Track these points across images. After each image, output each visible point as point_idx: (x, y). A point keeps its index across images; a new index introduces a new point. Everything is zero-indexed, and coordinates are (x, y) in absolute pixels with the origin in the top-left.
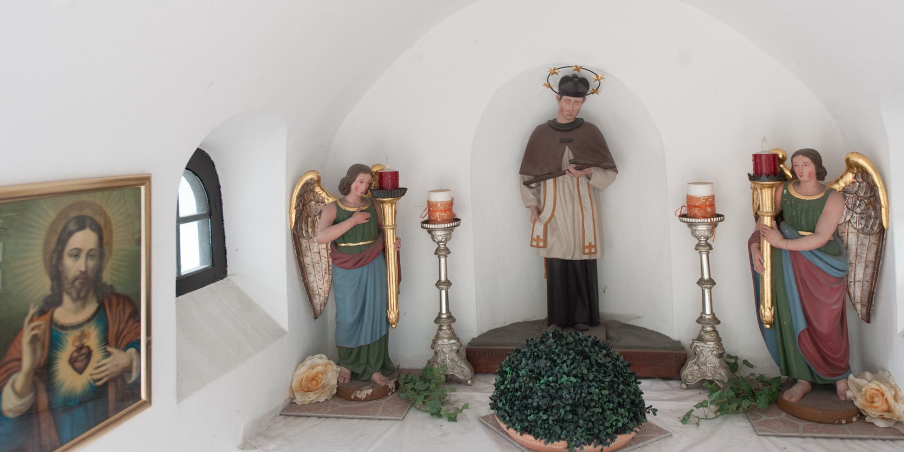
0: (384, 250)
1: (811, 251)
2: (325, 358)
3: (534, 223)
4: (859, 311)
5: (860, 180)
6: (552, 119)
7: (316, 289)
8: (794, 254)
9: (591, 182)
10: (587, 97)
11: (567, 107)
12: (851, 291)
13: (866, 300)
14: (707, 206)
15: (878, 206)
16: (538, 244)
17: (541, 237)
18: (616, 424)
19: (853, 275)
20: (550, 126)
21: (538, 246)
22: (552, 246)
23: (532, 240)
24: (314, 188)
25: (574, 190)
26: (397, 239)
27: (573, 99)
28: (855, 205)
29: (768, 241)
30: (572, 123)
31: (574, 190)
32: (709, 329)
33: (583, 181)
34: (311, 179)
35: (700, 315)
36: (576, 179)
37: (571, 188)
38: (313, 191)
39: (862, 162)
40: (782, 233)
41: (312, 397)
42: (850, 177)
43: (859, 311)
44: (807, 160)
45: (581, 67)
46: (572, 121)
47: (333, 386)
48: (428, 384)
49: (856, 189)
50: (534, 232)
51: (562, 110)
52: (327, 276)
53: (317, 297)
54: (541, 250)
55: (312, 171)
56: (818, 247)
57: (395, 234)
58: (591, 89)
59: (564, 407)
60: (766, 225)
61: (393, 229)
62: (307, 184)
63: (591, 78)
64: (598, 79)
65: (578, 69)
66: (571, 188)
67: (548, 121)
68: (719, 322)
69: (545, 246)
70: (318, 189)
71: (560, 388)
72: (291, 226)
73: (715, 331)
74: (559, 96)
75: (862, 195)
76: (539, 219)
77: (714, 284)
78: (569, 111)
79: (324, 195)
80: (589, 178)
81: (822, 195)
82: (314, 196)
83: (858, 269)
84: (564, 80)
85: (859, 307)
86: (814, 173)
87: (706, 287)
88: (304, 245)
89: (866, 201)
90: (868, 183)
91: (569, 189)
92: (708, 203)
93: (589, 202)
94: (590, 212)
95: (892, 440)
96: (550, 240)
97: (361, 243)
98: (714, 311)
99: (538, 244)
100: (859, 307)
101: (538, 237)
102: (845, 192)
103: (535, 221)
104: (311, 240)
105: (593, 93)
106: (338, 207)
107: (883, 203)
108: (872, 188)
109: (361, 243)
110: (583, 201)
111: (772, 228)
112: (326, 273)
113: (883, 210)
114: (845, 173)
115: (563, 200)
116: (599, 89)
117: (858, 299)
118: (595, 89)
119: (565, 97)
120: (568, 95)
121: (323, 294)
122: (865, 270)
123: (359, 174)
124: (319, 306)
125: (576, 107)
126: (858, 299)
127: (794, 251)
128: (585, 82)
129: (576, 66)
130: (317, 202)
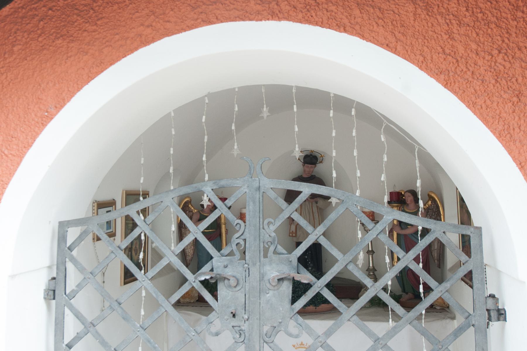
0: (220, 235)
1: (411, 234)
2: (212, 263)
3: (291, 225)
4: (436, 263)
5: (434, 203)
6: (300, 175)
7: (187, 253)
8: (405, 236)
9: (318, 205)
10: (317, 165)
11: (307, 169)
12: (433, 254)
13: (438, 258)
14: (370, 216)
15: (440, 215)
16: (292, 235)
17: (294, 231)
18: (322, 299)
19: (433, 247)
20: (299, 178)
21: (292, 236)
22: (299, 236)
23: (290, 233)
24: (188, 205)
25: (310, 209)
26: (226, 230)
27: (310, 166)
28: (432, 215)
29: (395, 231)
30: (310, 177)
31: (310, 209)
32: (371, 273)
33: (314, 205)
34: (188, 201)
35: (367, 268)
36: (311, 203)
37: (309, 209)
38: (188, 206)
39: (433, 195)
40: (401, 227)
41: (187, 300)
42: (430, 202)
43: (436, 263)
44: (409, 194)
45: (313, 151)
46: (310, 176)
47: (196, 296)
48: (362, 14)
49: (433, 207)
50: (291, 229)
51: (305, 171)
52: (192, 247)
53: (188, 256)
54: (294, 238)
55: (188, 197)
56: (414, 232)
57: (225, 227)
58: (319, 161)
59: (301, 291)
60: (395, 224)
61: (225, 224)
62: (186, 203)
63: (319, 156)
64: (322, 156)
65: (312, 151)
66: (309, 209)
67: (298, 176)
68: (376, 270)
69: (296, 236)
70: (190, 206)
71: (299, 284)
72: (178, 222)
73: (374, 274)
74: (303, 164)
75: (435, 210)
76: (293, 223)
77: (374, 252)
78: (308, 171)
79: (192, 208)
80: (317, 203)
81: (416, 210)
82: (188, 209)
83: (435, 244)
84: (306, 157)
85: (436, 261)
86: (413, 200)
87: (370, 254)
88: (183, 232)
89: (436, 213)
90: (436, 205)
91: (308, 209)
92: (370, 215)
93: (317, 215)
94: (318, 220)
95: (440, 312)
96: (298, 233)
97: (210, 231)
98: (374, 266)
99: (292, 235)
100: (436, 261)
101: (293, 231)
102: (428, 209)
103: (291, 224)
104: (186, 229)
105: (320, 163)
106: (200, 213)
107: (442, 213)
108: (438, 207)
109: (210, 231)
110: (314, 215)
111: (397, 225)
112: (192, 245)
113: (442, 216)
114: (428, 201)
115: (305, 213)
116: (323, 161)
117: (436, 258)
118: (321, 161)
119: (306, 165)
120: (307, 164)
121: (190, 256)
122: (438, 244)
123: (336, 175)
124: (188, 261)
125: (312, 170)
126: (436, 258)
127: (405, 235)
128: (316, 158)
129: (311, 150)
130: (190, 212)
